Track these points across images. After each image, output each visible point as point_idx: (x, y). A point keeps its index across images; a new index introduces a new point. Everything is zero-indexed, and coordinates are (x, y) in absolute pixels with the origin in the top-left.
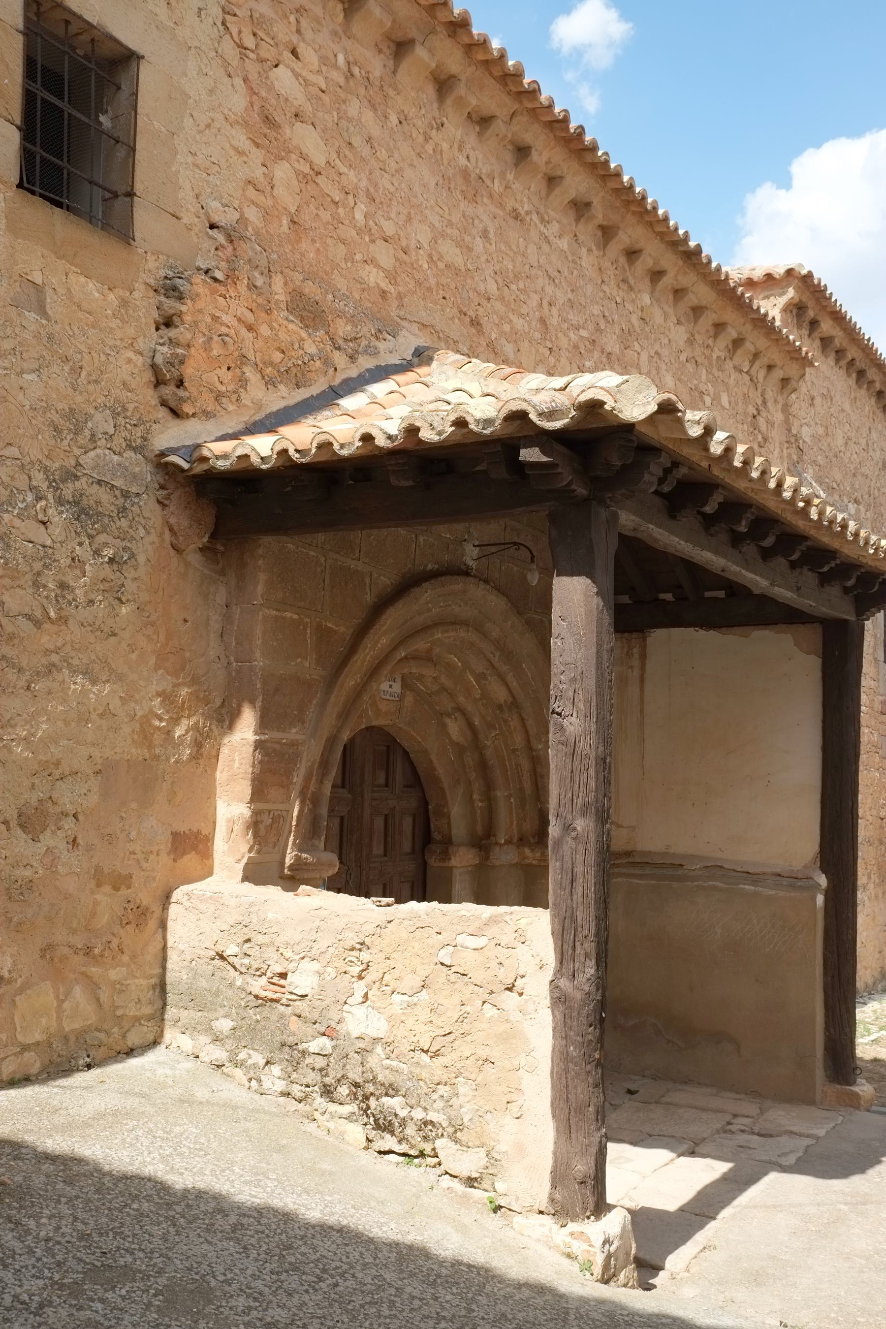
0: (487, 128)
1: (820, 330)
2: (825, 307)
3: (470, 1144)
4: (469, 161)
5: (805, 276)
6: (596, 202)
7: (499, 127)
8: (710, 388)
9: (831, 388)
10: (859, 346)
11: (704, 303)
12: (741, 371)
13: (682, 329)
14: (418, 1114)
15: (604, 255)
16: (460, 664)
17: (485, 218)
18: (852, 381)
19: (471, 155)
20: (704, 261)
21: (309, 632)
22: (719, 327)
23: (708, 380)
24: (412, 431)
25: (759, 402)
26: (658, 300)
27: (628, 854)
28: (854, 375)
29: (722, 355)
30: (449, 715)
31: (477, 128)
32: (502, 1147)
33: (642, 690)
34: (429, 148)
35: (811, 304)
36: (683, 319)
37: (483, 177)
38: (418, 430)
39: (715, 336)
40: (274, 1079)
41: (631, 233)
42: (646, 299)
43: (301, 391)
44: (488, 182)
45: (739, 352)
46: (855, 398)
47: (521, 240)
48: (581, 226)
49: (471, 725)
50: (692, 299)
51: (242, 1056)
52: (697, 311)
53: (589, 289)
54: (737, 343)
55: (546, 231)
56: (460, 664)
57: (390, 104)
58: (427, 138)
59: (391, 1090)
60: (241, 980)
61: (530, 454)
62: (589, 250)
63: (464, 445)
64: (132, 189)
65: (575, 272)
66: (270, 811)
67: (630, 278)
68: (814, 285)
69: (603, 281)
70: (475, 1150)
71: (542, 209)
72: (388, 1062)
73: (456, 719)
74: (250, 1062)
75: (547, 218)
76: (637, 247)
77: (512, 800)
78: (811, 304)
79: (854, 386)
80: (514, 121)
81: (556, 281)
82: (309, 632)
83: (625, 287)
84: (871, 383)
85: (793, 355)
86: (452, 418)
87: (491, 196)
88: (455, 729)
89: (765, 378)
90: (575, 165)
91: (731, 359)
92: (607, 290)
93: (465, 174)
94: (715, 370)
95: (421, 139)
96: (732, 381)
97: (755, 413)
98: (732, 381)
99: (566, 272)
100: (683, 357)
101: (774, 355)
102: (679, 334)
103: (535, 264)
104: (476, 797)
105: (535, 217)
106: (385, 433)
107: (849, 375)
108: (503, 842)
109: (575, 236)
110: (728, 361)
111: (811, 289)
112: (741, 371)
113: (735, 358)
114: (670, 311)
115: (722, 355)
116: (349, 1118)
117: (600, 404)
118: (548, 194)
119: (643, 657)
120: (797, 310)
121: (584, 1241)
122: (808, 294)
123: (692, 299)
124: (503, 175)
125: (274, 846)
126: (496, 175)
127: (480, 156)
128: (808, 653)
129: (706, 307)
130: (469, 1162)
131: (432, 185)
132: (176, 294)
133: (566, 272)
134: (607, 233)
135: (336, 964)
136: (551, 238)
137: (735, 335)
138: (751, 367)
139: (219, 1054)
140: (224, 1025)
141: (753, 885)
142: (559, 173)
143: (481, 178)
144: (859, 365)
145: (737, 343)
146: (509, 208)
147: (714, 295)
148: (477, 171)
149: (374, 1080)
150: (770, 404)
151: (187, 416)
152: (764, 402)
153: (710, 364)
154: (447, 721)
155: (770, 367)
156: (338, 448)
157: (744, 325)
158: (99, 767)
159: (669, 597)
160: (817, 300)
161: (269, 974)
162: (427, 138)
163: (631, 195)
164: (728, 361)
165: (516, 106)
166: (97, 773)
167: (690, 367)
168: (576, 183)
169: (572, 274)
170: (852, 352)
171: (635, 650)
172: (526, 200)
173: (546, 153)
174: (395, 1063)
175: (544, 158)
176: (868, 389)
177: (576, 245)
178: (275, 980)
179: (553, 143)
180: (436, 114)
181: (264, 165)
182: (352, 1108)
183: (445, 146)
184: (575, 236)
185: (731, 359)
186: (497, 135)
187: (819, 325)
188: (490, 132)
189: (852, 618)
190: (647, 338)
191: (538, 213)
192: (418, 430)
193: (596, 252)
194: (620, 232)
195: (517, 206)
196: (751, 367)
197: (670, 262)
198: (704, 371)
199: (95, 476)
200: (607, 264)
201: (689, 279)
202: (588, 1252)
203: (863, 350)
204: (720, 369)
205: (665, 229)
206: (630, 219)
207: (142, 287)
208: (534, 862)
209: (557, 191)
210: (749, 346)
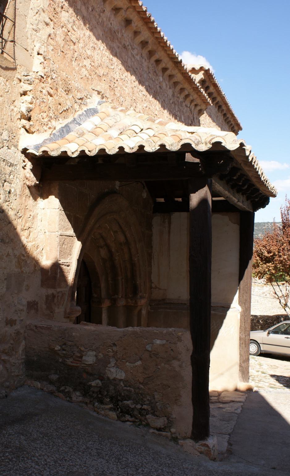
0: (118, 13)
1: (209, 90)
2: (211, 81)
3: (160, 416)
4: (111, 25)
5: (207, 70)
6: (150, 41)
7: (122, 13)
8: (179, 114)
9: (211, 112)
10: (220, 96)
11: (179, 81)
12: (187, 107)
13: (171, 91)
14: (139, 406)
15: (149, 62)
16: (108, 228)
17: (116, 48)
18: (217, 109)
19: (112, 23)
20: (183, 65)
21: (72, 219)
22: (182, 90)
23: (178, 111)
24: (141, 147)
25: (192, 119)
26: (164, 79)
27: (164, 300)
28: (217, 107)
29: (182, 100)
30: (102, 247)
31: (114, 12)
32: (174, 416)
33: (169, 236)
34: (100, 20)
35: (207, 80)
36: (171, 87)
37: (116, 31)
38: (144, 147)
39: (180, 93)
40: (77, 396)
41: (160, 54)
42: (161, 79)
43: (66, 120)
44: (117, 33)
45: (188, 99)
46: (218, 116)
47: (126, 56)
48: (143, 51)
49: (110, 251)
50: (175, 80)
51: (63, 388)
52: (176, 84)
53: (145, 75)
54: (187, 96)
55: (133, 53)
56: (108, 228)
57: (89, 3)
58: (100, 15)
59: (128, 398)
60: (61, 359)
61: (189, 157)
62: (145, 60)
63: (160, 153)
64: (14, 39)
65: (141, 69)
66: (61, 292)
67: (157, 71)
68: (210, 74)
69: (149, 72)
70: (162, 418)
71: (132, 44)
72: (126, 388)
73: (104, 249)
74: (66, 390)
75: (133, 48)
76: (161, 59)
77: (123, 280)
78: (207, 80)
79: (217, 112)
80: (128, 10)
81: (136, 72)
82: (72, 219)
83: (155, 74)
84: (223, 110)
85: (204, 101)
86: (160, 143)
87: (118, 39)
88: (103, 253)
89: (194, 109)
90: (145, 28)
91: (185, 102)
92: (150, 76)
93: (110, 30)
94: (180, 107)
95: (98, 17)
96: (185, 111)
97: (191, 123)
98: (185, 111)
99: (139, 68)
100: (171, 102)
101: (199, 101)
102: (170, 92)
103: (130, 66)
104: (109, 279)
105: (130, 47)
106: (129, 147)
107: (216, 107)
108: (120, 297)
109: (141, 54)
110: (184, 103)
111: (208, 75)
112: (187, 107)
113: (186, 102)
114: (167, 83)
115: (182, 100)
116: (110, 409)
117: (220, 143)
118: (134, 38)
119: (170, 223)
120: (202, 82)
121: (206, 447)
122: (207, 77)
123: (175, 80)
124: (121, 30)
125: (62, 305)
126: (119, 31)
127: (115, 23)
128: (234, 223)
129: (179, 82)
130: (160, 422)
131: (101, 35)
132: (29, 82)
133: (139, 68)
134: (151, 53)
135: (103, 352)
136: (135, 55)
137: (187, 93)
138: (190, 105)
139: (52, 388)
140: (54, 377)
141: (214, 311)
142: (139, 30)
143: (115, 32)
144: (220, 104)
145: (187, 96)
146: (123, 44)
147: (182, 78)
148: (114, 30)
149: (120, 395)
150: (195, 119)
151: (33, 133)
152: (194, 119)
153: (179, 104)
154: (101, 249)
155: (196, 105)
156: (108, 151)
157: (191, 89)
158: (6, 277)
159: (180, 200)
160: (210, 79)
161: (74, 357)
162: (100, 15)
163: (163, 40)
164: (184, 103)
165: (129, 5)
166: (5, 279)
167: (173, 105)
168: (145, 35)
169: (140, 69)
170: (219, 99)
171: (166, 220)
172: (128, 40)
173: (137, 23)
174: (128, 388)
175: (136, 24)
176: (221, 113)
177: (141, 58)
178: (77, 359)
179: (139, 19)
180: (102, 6)
181: (53, 29)
182: (111, 406)
183: (105, 19)
184: (141, 54)
185: (185, 102)
186: (121, 15)
187: (209, 88)
188: (119, 14)
189: (252, 211)
190: (161, 95)
191: (131, 46)
192: (144, 147)
193: (147, 61)
194: (156, 54)
195: (125, 43)
196: (190, 105)
197: (170, 65)
198: (177, 107)
199: (3, 158)
200: (150, 66)
201: (175, 72)
202: (208, 450)
203: (221, 98)
204: (181, 106)
205: (172, 53)
206: (160, 49)
207: (16, 79)
208: (132, 305)
209: (138, 37)
210: (191, 98)
